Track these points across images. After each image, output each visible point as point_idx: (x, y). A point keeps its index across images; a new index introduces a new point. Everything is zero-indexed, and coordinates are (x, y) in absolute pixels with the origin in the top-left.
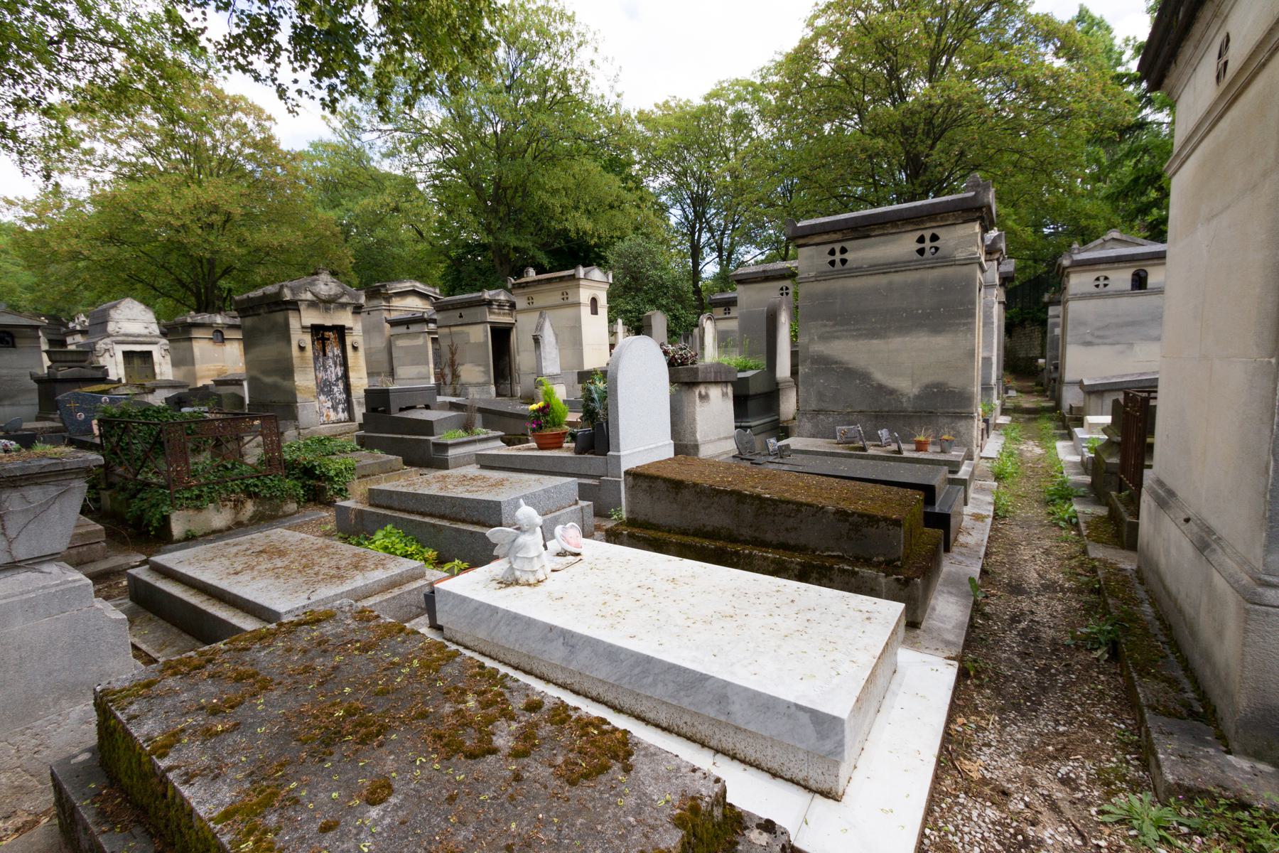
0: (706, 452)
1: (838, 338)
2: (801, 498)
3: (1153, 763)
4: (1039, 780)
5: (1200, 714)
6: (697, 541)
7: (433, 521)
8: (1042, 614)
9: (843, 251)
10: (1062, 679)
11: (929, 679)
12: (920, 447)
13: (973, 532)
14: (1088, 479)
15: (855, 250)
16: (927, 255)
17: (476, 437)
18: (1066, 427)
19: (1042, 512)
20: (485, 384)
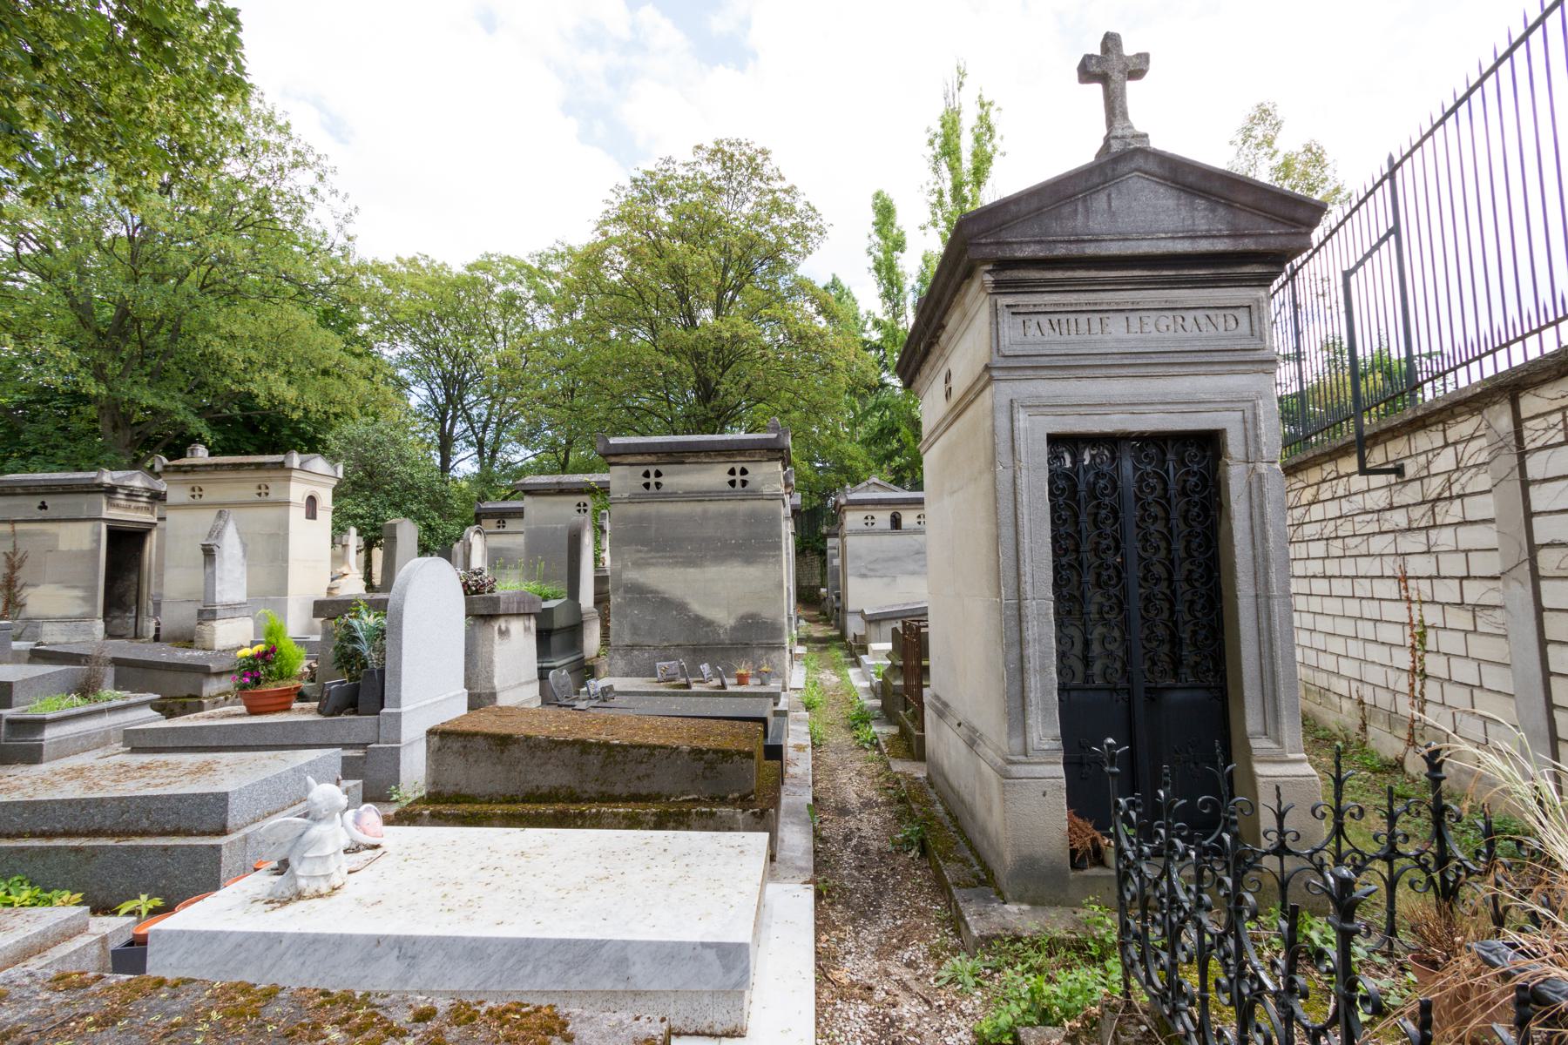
0: (504, 700)
1: (653, 565)
2: (653, 741)
3: (962, 926)
4: (892, 969)
5: (986, 882)
6: (530, 808)
7: (76, 842)
8: (866, 830)
9: (658, 474)
10: (891, 881)
11: (795, 902)
12: (742, 680)
13: (799, 765)
14: (878, 703)
15: (669, 474)
16: (739, 485)
17: (105, 705)
18: (853, 655)
19: (849, 736)
20: (82, 618)
